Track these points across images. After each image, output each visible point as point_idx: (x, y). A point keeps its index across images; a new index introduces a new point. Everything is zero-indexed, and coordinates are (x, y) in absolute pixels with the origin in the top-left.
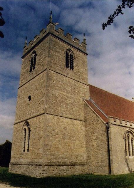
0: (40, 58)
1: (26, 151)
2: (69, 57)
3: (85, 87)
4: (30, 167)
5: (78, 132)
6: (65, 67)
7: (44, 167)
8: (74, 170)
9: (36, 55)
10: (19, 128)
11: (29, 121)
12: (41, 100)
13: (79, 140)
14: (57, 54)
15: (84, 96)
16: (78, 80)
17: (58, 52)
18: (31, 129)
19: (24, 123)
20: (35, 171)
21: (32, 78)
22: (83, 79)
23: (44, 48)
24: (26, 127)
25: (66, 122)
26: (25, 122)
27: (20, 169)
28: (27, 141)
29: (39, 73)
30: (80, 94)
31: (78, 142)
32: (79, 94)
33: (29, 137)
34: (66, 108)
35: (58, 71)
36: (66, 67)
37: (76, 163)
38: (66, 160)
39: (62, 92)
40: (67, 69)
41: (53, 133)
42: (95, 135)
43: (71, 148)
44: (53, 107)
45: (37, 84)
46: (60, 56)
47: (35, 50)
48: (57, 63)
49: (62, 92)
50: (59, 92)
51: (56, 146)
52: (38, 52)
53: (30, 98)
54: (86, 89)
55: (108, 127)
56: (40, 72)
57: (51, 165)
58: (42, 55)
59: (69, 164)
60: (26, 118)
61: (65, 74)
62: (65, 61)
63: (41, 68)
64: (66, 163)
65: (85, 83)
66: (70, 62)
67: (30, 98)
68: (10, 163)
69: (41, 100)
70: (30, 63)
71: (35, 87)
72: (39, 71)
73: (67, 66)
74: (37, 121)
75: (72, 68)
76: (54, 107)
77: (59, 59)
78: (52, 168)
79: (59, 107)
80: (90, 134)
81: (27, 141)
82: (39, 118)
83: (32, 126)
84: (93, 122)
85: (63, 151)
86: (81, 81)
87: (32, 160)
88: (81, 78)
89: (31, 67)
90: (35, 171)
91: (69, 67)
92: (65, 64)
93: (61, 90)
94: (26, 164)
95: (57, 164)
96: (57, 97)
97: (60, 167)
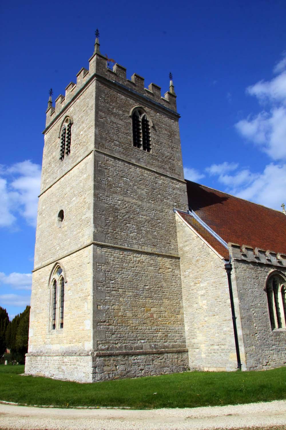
0: (78, 131)
1: (58, 326)
2: (140, 129)
3: (178, 186)
4: (66, 359)
5: (166, 281)
6: (132, 145)
7: (96, 359)
8: (161, 362)
9: (71, 124)
10: (43, 280)
11: (63, 263)
12: (83, 218)
13: (168, 299)
14: (113, 118)
15: (175, 204)
16: (161, 171)
17: (115, 115)
18: (68, 279)
19: (51, 269)
20: (77, 368)
21: (64, 174)
22: (172, 169)
23: (85, 108)
24: (56, 277)
25: (139, 261)
26: (53, 265)
27: (47, 364)
28: (58, 305)
29: (77, 162)
30: (168, 201)
31: (166, 302)
32: (165, 201)
33: (62, 296)
34: (139, 230)
35: (117, 155)
36: (135, 145)
37: (165, 347)
38: (143, 341)
39: (126, 199)
40: (136, 149)
41: (111, 285)
42: (202, 285)
43: (152, 316)
44: (109, 231)
45: (74, 184)
46: (121, 122)
47: (67, 113)
48: (115, 137)
49: (126, 199)
50: (121, 197)
51: (120, 314)
52: (75, 119)
53: (61, 215)
54: (179, 189)
55: (229, 267)
56: (80, 160)
57: (110, 355)
58: (83, 122)
59: (151, 350)
60: (55, 258)
61: (133, 161)
62: (132, 132)
63: (82, 151)
64: (142, 348)
65: (176, 177)
66: (141, 135)
67: (61, 215)
68: (26, 354)
69: (83, 218)
70: (59, 141)
71: (72, 191)
72: (78, 157)
73: (136, 143)
74: (78, 262)
75: (147, 147)
76: (112, 231)
77: (118, 130)
78: (112, 361)
79: (122, 230)
80: (192, 284)
81: (58, 305)
82: (70, 250)
83: (68, 273)
84: (198, 258)
85: (133, 322)
86: (168, 174)
87: (70, 345)
88: (167, 167)
89: (61, 150)
90: (77, 368)
91: (141, 145)
92: (131, 138)
93: (125, 194)
94: (57, 354)
95: (124, 351)
96: (116, 209)
97: (130, 358)
